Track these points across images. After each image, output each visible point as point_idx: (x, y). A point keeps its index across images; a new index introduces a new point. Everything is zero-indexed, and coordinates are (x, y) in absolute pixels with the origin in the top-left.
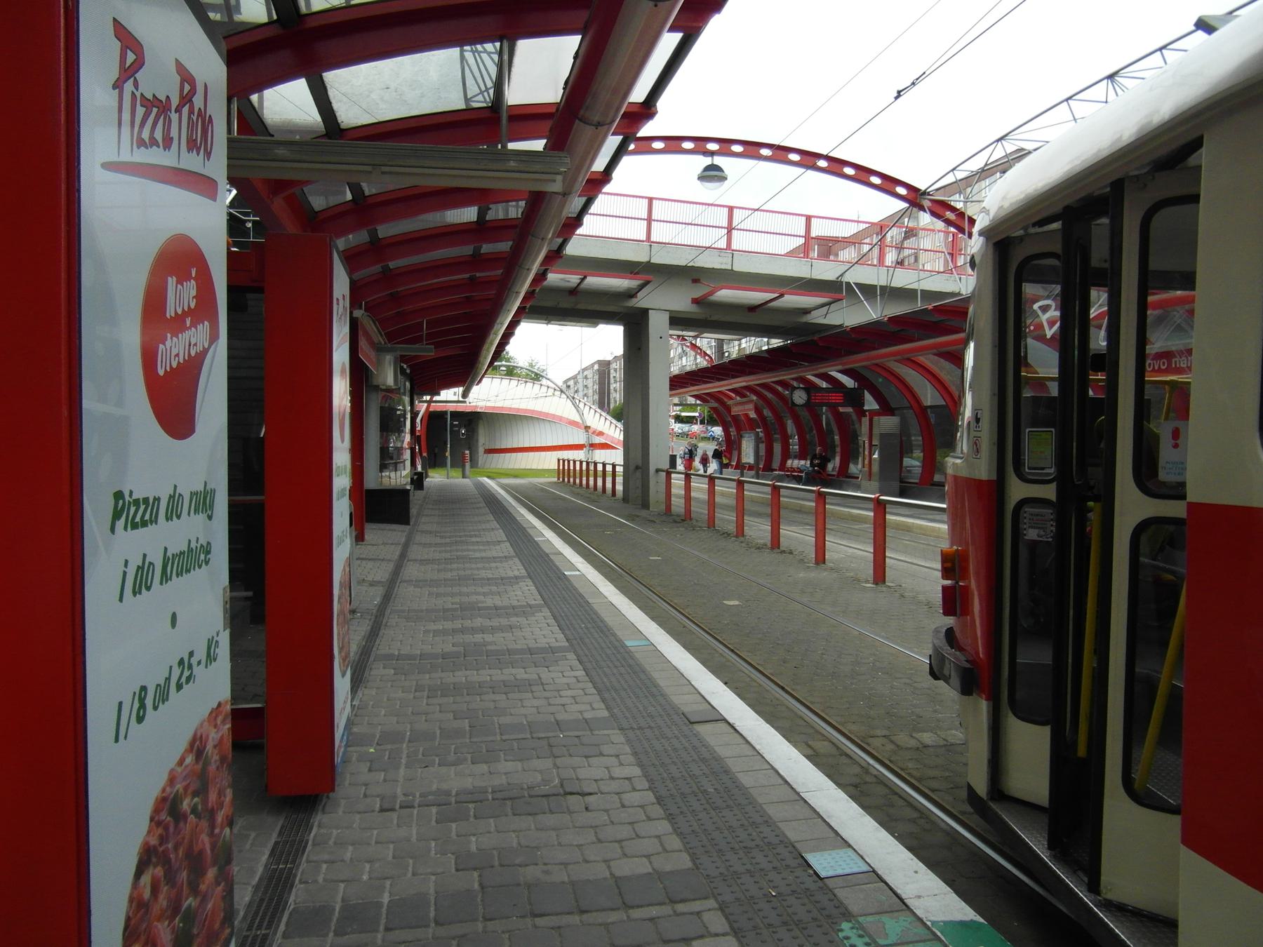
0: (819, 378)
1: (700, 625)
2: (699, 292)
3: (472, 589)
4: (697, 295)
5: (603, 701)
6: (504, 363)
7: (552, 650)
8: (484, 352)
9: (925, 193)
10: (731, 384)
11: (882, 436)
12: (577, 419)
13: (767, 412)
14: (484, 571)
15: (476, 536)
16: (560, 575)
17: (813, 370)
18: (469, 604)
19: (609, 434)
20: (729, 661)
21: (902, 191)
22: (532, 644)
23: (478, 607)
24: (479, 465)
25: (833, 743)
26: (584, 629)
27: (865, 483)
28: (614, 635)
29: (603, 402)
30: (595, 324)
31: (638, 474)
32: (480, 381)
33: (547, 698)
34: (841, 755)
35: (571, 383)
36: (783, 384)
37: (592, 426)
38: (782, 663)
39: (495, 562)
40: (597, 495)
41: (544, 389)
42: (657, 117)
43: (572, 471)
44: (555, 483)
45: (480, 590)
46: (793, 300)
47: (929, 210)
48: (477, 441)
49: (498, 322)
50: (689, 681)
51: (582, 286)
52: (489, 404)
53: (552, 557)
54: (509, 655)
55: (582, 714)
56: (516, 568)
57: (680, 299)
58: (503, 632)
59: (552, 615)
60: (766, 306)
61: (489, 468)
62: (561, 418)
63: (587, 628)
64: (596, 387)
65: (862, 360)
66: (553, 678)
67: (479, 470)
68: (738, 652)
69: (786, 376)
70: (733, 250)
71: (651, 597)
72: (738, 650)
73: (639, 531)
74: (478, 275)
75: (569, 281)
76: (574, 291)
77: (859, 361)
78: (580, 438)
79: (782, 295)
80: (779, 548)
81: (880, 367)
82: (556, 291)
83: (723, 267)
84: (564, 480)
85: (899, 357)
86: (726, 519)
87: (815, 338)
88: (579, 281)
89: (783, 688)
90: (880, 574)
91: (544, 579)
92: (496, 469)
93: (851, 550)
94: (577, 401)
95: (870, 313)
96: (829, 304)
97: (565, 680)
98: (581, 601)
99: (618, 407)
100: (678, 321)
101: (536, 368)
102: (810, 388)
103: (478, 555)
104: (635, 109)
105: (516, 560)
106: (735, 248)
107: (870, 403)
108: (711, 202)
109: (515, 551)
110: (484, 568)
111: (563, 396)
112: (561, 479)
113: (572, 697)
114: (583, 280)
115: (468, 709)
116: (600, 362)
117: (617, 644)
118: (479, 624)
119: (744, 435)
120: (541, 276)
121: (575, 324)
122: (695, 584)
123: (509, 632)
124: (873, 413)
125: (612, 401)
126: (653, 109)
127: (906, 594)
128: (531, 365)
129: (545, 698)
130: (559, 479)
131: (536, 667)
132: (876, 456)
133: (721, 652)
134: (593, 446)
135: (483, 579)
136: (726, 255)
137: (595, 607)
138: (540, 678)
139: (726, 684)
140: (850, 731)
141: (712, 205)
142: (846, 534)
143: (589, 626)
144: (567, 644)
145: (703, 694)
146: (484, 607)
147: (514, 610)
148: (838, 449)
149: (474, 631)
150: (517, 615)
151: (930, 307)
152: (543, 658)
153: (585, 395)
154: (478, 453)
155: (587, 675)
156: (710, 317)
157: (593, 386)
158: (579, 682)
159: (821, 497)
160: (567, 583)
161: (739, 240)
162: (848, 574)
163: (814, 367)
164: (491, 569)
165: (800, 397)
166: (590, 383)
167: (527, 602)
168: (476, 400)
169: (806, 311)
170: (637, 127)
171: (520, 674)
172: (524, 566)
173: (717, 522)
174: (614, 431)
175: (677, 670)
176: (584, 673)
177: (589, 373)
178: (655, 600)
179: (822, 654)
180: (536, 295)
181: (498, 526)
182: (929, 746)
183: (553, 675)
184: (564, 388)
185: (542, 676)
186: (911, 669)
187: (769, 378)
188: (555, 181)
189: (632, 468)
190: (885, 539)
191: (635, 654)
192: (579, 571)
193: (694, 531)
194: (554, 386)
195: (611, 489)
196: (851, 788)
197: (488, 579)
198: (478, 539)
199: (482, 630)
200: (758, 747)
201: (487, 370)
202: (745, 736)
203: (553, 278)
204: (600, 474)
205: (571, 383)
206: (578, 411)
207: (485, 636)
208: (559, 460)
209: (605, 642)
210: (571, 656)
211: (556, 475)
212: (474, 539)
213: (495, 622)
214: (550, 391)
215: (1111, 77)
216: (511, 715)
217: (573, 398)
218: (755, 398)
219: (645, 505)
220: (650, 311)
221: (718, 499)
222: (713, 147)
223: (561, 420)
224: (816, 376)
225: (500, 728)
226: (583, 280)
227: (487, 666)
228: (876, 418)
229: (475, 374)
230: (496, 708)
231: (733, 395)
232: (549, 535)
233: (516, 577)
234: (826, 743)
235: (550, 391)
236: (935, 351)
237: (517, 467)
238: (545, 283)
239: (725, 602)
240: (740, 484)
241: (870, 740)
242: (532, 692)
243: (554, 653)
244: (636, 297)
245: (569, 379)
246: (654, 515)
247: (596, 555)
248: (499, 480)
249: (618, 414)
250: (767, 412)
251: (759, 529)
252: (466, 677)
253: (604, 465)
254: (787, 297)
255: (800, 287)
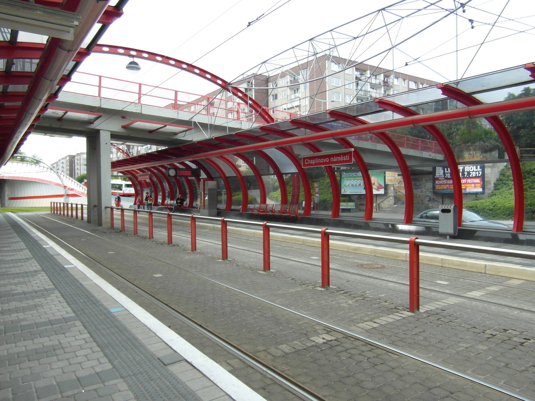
0: (181, 165)
1: (145, 290)
2: (125, 123)
3: (6, 281)
4: (124, 124)
5: (106, 356)
6: (18, 155)
7: (66, 320)
8: (9, 148)
9: (229, 84)
10: (139, 166)
11: (209, 190)
12: (60, 183)
13: (155, 179)
14: (14, 269)
15: (7, 247)
16: (62, 268)
17: (178, 161)
18: (6, 292)
19: (77, 189)
20: (166, 312)
21: (220, 82)
22: (52, 318)
23: (12, 294)
24: (6, 205)
25: (240, 360)
26: (83, 303)
27: (202, 210)
28: (102, 305)
29: (72, 174)
30: (71, 136)
31: (96, 209)
32: (5, 164)
33: (68, 359)
34: (247, 367)
35: (55, 165)
36: (163, 166)
37: (67, 186)
38: (195, 310)
39: (20, 262)
40: (73, 220)
41: (42, 168)
42: (123, 17)
43: (55, 208)
44: (50, 214)
45: (12, 281)
46: (170, 128)
47: (232, 92)
48: (4, 193)
49: (19, 131)
50: (155, 333)
51: (65, 117)
52: (11, 175)
53: (55, 257)
54: (37, 327)
55: (94, 369)
56: (34, 265)
57: (116, 126)
58: (30, 311)
59: (61, 295)
60: (157, 131)
61: (12, 207)
62: (51, 182)
63: (84, 302)
64: (68, 167)
65: (201, 157)
66: (69, 342)
67: (6, 208)
68: (170, 305)
69: (166, 163)
70: (141, 104)
71: (114, 276)
72: (170, 304)
73: (99, 238)
74: (3, 115)
75: (57, 114)
76: (60, 119)
77: (199, 157)
78: (62, 192)
79: (165, 126)
80: (172, 243)
81: (208, 159)
82: (50, 118)
83: (137, 111)
84: (54, 212)
85: (235, 153)
86: (144, 230)
87: (180, 146)
88: (63, 114)
89: (200, 326)
90: (225, 255)
91: (53, 271)
92: (15, 207)
93: (205, 243)
94: (60, 174)
95: (205, 136)
96: (186, 131)
97: (77, 343)
98: (77, 284)
99: (79, 177)
100: (115, 136)
101: (36, 157)
102: (176, 168)
103: (9, 258)
104: (110, 9)
105: (34, 260)
106: (142, 103)
107: (203, 175)
108: (132, 81)
109: (32, 255)
110: (14, 267)
111: (52, 171)
112: (53, 212)
113: (84, 355)
114: (65, 113)
115: (10, 378)
116: (70, 156)
117: (105, 311)
118: (14, 306)
119: (144, 190)
120: (44, 108)
121: (60, 136)
122: (136, 266)
123: (34, 310)
124: (205, 180)
125: (76, 174)
126: (121, 11)
127: (239, 264)
128: (34, 156)
129: (66, 359)
130: (51, 212)
131: (56, 334)
132: (207, 198)
133: (161, 306)
134: (68, 195)
135: (14, 274)
136: (138, 106)
137: (87, 287)
138: (60, 343)
139: (169, 327)
140: (245, 350)
141: (132, 82)
142: (205, 235)
143: (85, 300)
144: (74, 315)
145: (166, 342)
146: (16, 293)
147: (36, 294)
148: (188, 196)
149: (10, 311)
150: (39, 297)
151: (234, 133)
152: (60, 327)
153: (62, 171)
154: (5, 200)
155: (91, 337)
156: (131, 134)
157: (66, 167)
158: (86, 342)
159: (224, 223)
160: (67, 273)
161: (144, 100)
162: (208, 255)
163: (178, 159)
164: (18, 267)
165: (172, 173)
166: (65, 165)
167: (44, 287)
168: (3, 173)
169: (176, 134)
170: (111, 20)
171: (46, 341)
172: (39, 263)
173: (125, 228)
174: (81, 189)
175: (146, 326)
176: (88, 335)
177: (64, 161)
178: (117, 278)
179: (213, 302)
180: (40, 119)
181: (20, 240)
182: (288, 353)
183: (69, 339)
184: (51, 167)
185: (62, 341)
186: (259, 306)
187: (157, 164)
188: (69, 32)
189: (92, 206)
190: (227, 238)
191: (118, 317)
192: (72, 264)
193: (127, 237)
194: (47, 167)
195: (75, 216)
196: (262, 391)
197: (17, 274)
198: (9, 249)
199: (17, 310)
200: (212, 379)
201: (10, 158)
202: (161, 337)
203: (49, 112)
204: (70, 208)
205: (55, 165)
206: (60, 179)
207: (19, 314)
208: (51, 203)
209: (98, 311)
210: (78, 323)
211: (50, 210)
212: (6, 249)
213: (24, 304)
214: (45, 169)
215: (310, 40)
216: (44, 378)
217: (58, 172)
218: (149, 173)
219: (100, 224)
220: (101, 131)
221: (138, 220)
222: (133, 53)
223: (51, 183)
224: (179, 163)
225: (36, 392)
226: (65, 113)
227: (22, 339)
228: (206, 182)
229: (3, 159)
230: (31, 373)
231: (139, 172)
232: (51, 244)
233: (35, 271)
234: (236, 360)
235: (45, 169)
236: (276, 146)
237: (27, 206)
238: (57, 99)
239: (154, 275)
240: (151, 214)
241: (259, 354)
242: (56, 355)
243: (66, 322)
244: (94, 124)
245: (54, 164)
246: (105, 229)
247: (79, 253)
248: (18, 213)
249: (80, 180)
250: (155, 179)
251: (161, 234)
252: (7, 350)
253: (72, 204)
254: (168, 127)
255: (173, 123)
